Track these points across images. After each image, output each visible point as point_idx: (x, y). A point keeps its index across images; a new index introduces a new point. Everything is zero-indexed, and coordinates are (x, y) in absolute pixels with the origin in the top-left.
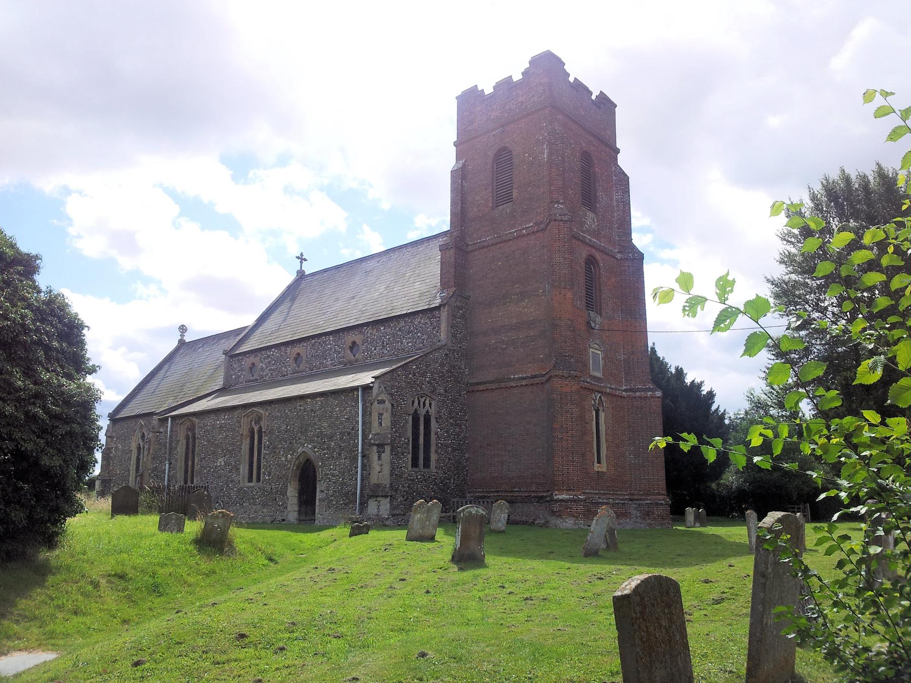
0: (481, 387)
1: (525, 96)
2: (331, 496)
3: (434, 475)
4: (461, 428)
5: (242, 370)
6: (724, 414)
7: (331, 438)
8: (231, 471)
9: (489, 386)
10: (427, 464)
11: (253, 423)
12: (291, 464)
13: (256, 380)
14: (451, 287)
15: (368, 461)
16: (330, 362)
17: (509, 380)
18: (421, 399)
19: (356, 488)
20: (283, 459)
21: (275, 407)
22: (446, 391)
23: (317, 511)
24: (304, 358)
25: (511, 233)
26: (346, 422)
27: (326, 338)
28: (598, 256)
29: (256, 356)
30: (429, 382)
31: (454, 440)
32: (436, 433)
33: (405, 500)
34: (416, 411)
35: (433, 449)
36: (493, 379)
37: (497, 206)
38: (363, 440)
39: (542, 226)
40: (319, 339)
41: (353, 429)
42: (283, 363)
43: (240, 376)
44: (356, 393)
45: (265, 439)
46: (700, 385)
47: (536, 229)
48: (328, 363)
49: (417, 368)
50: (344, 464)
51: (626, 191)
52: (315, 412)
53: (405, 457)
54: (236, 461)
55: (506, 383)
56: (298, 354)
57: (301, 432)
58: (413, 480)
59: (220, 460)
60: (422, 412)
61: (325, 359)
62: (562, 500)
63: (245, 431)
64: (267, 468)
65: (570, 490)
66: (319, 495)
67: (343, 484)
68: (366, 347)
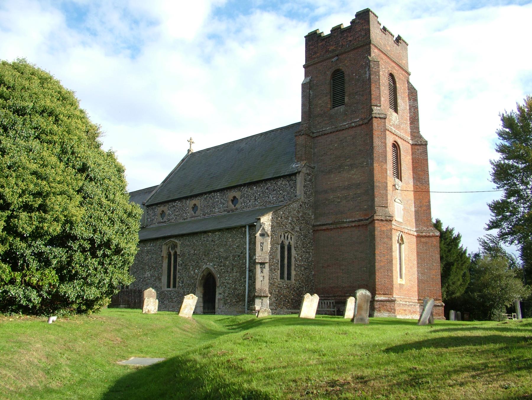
0: (324, 227)
1: (352, 37)
2: (227, 297)
3: (293, 285)
4: (309, 255)
5: (155, 215)
6: (466, 250)
7: (226, 258)
8: (155, 280)
9: (328, 227)
10: (289, 278)
11: (170, 249)
12: (198, 276)
13: (165, 222)
14: (303, 160)
15: (253, 274)
16: (217, 210)
17: (343, 222)
18: (285, 234)
19: (245, 292)
20: (192, 273)
21: (186, 238)
22: (300, 230)
23: (217, 306)
24: (199, 207)
25: (344, 125)
26: (237, 248)
27: (214, 194)
28: (400, 142)
29: (165, 206)
30: (290, 223)
31: (305, 262)
32: (295, 258)
33: (276, 300)
34: (282, 242)
35: (293, 267)
36: (331, 222)
37: (333, 108)
38: (249, 260)
39: (366, 121)
40: (209, 195)
41: (241, 253)
42: (184, 211)
43: (153, 220)
44: (244, 229)
45: (179, 260)
46: (452, 230)
47: (361, 123)
48: (216, 211)
49: (283, 213)
50: (236, 276)
51: (416, 100)
52: (214, 242)
53: (276, 272)
54: (158, 274)
55: (341, 225)
56: (195, 205)
57: (205, 255)
58: (281, 288)
59: (147, 273)
60: (286, 243)
61: (214, 208)
62: (381, 301)
63: (164, 254)
64: (181, 279)
65: (386, 294)
66: (218, 296)
67: (235, 289)
68: (244, 200)
